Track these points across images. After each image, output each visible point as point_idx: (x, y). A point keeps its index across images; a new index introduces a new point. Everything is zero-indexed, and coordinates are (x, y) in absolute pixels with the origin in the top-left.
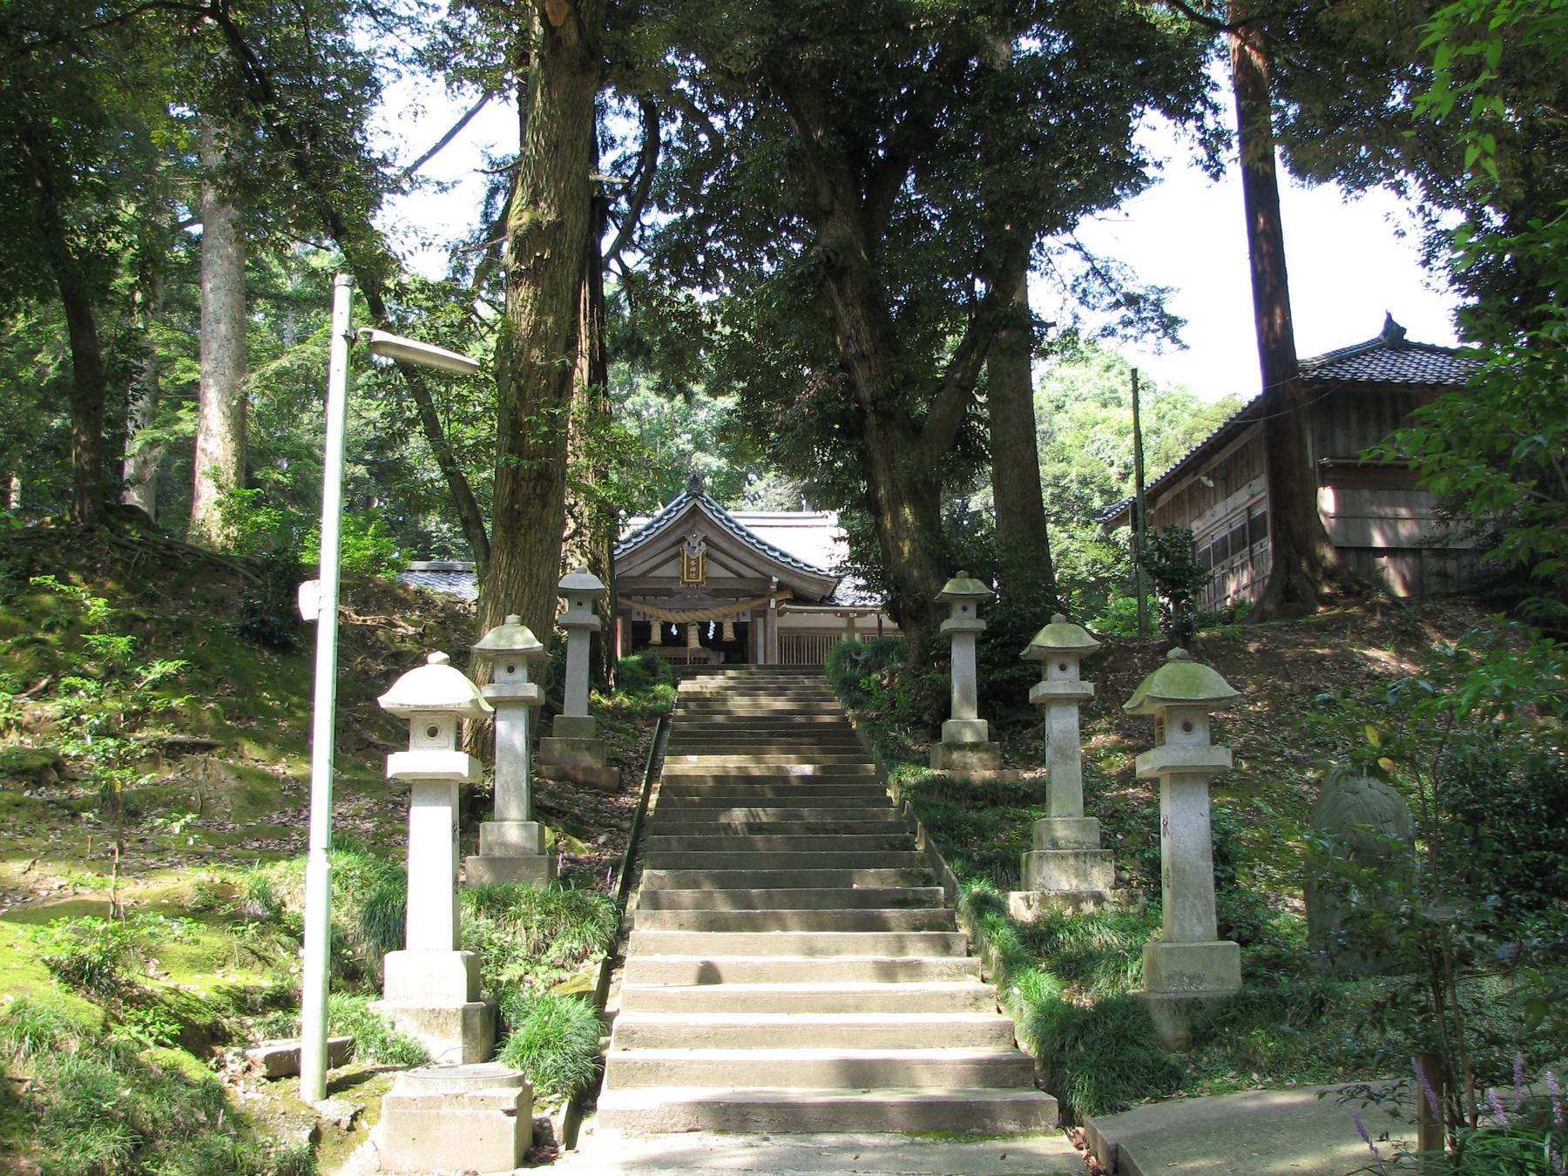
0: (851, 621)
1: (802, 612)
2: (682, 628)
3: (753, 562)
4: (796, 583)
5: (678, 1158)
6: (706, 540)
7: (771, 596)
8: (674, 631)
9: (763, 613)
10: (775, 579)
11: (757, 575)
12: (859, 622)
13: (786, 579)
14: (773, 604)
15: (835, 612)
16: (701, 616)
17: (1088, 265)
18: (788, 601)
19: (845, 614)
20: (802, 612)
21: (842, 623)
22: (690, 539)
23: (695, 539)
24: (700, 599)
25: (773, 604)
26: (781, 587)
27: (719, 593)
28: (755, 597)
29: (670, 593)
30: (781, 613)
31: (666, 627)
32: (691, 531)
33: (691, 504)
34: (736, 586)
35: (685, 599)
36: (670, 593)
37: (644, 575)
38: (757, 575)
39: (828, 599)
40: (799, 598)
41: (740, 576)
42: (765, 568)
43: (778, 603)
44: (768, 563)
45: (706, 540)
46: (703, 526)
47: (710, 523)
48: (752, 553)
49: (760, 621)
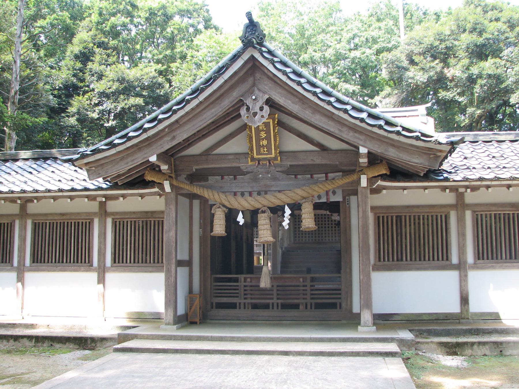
0: (460, 197)
1: (404, 188)
2: (253, 215)
3: (332, 127)
4: (392, 153)
5: (58, 346)
6: (269, 102)
7: (362, 171)
8: (241, 219)
9: (353, 190)
10: (363, 150)
11: (345, 146)
12: (470, 197)
13: (378, 149)
14: (364, 182)
15: (444, 188)
16: (273, 200)
17: (180, 23)
18: (383, 177)
19: (454, 189)
20: (404, 188)
21: (449, 198)
22: (248, 102)
23: (256, 102)
24: (275, 179)
25: (364, 182)
26: (374, 159)
27: (299, 170)
28: (347, 173)
29: (236, 173)
30: (377, 191)
31: (230, 216)
32: (250, 92)
33: (246, 57)
34: (319, 160)
35: (256, 179)
36: (236, 173)
37: (207, 152)
38: (345, 146)
39: (431, 174)
40: (398, 173)
41: (323, 148)
42: (349, 136)
43: (371, 181)
44: (353, 128)
45: (269, 102)
46: (266, 85)
47: (274, 79)
48: (330, 116)
49: (353, 200)
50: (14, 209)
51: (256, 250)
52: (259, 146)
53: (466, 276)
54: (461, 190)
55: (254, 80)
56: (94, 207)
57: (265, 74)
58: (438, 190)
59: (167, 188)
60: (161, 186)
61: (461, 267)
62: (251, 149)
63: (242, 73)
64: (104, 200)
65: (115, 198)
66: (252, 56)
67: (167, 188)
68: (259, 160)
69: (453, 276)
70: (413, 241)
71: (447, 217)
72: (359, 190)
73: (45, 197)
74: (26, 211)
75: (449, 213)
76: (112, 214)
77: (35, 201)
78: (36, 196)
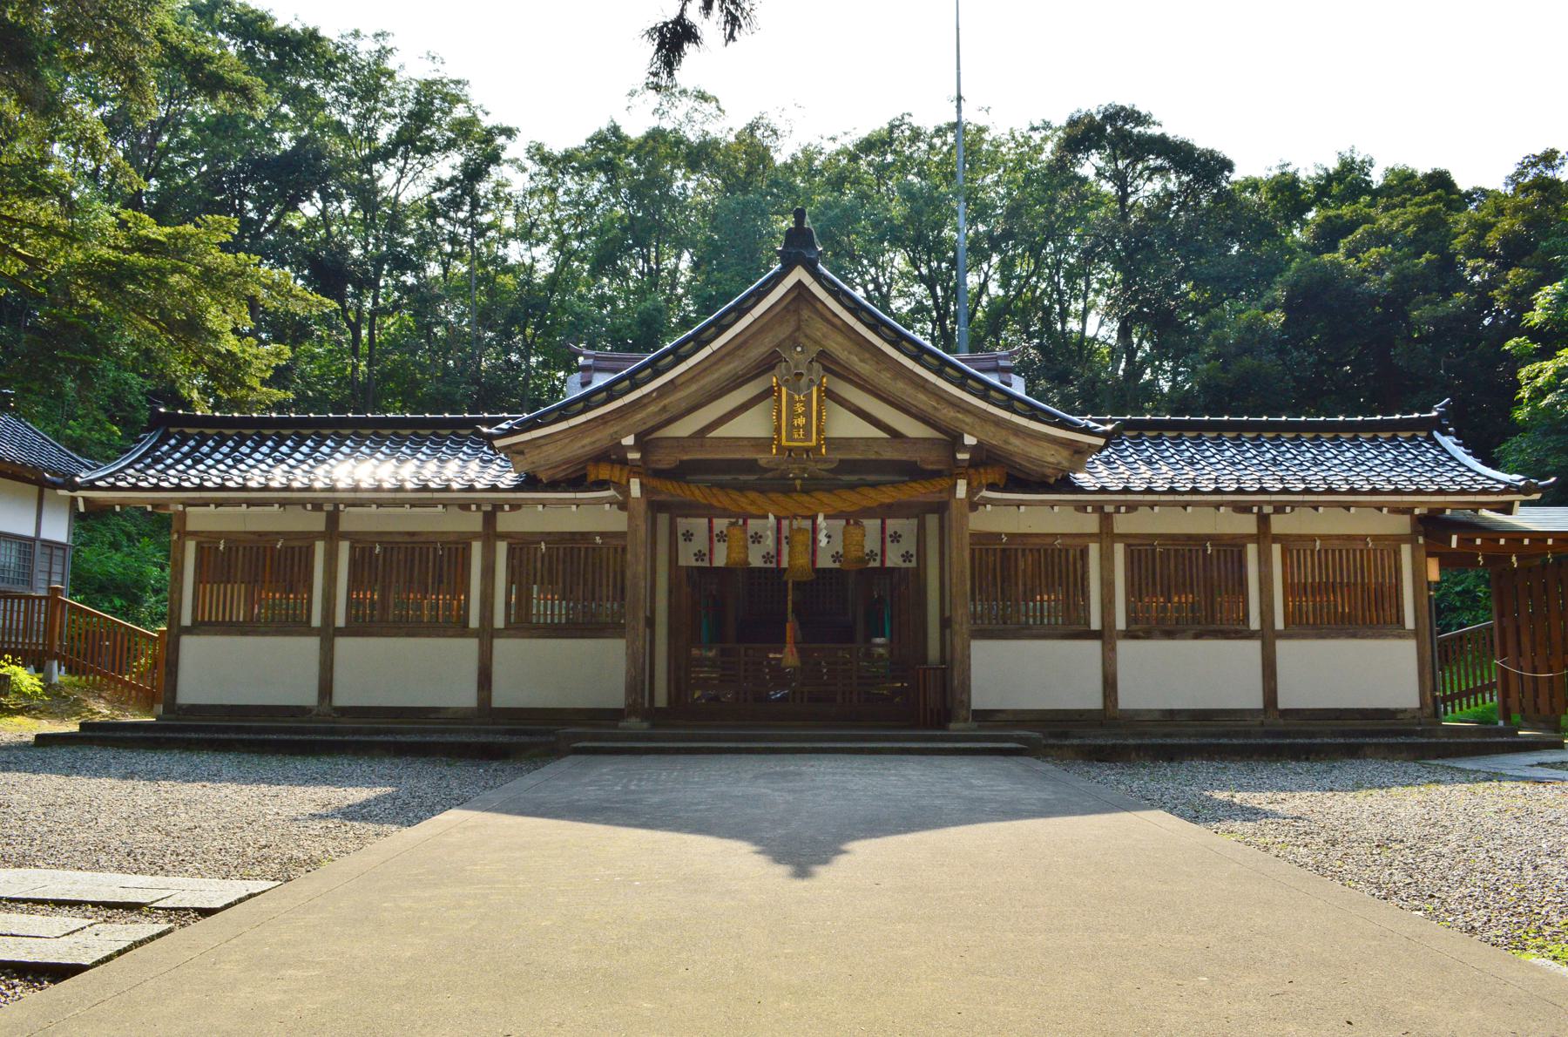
12: (1124, 524)
20: (1018, 504)
21: (1090, 523)
33: (789, 281)
34: (889, 454)
41: (895, 434)
43: (971, 490)
50: (317, 522)
51: (1492, 604)
52: (791, 427)
53: (1114, 649)
54: (1109, 509)
55: (799, 320)
56: (317, 522)
57: (817, 311)
58: (1071, 509)
59: (635, 488)
60: (624, 489)
61: (1105, 636)
62: (778, 430)
63: (778, 309)
64: (180, 508)
65: (516, 506)
66: (799, 284)
67: (635, 488)
68: (790, 450)
69: (1251, 650)
70: (1031, 588)
71: (1084, 553)
72: (954, 504)
73: (1303, 504)
74: (494, 527)
75: (1087, 547)
76: (194, 534)
77: (1288, 509)
78: (357, 499)
